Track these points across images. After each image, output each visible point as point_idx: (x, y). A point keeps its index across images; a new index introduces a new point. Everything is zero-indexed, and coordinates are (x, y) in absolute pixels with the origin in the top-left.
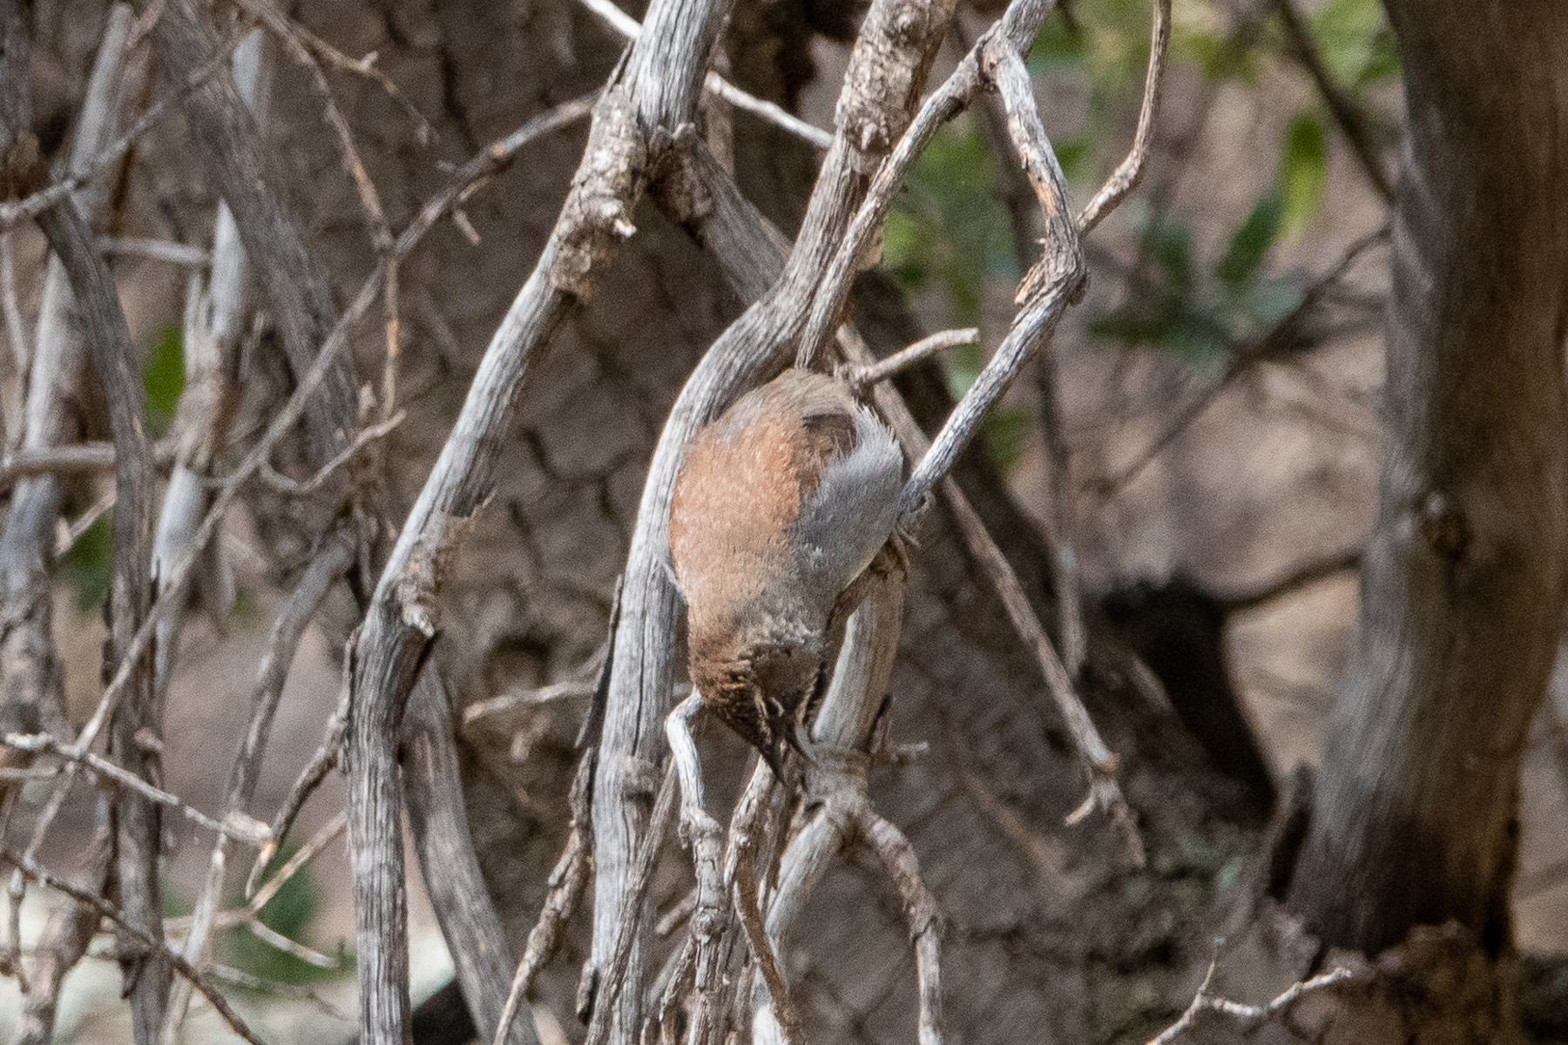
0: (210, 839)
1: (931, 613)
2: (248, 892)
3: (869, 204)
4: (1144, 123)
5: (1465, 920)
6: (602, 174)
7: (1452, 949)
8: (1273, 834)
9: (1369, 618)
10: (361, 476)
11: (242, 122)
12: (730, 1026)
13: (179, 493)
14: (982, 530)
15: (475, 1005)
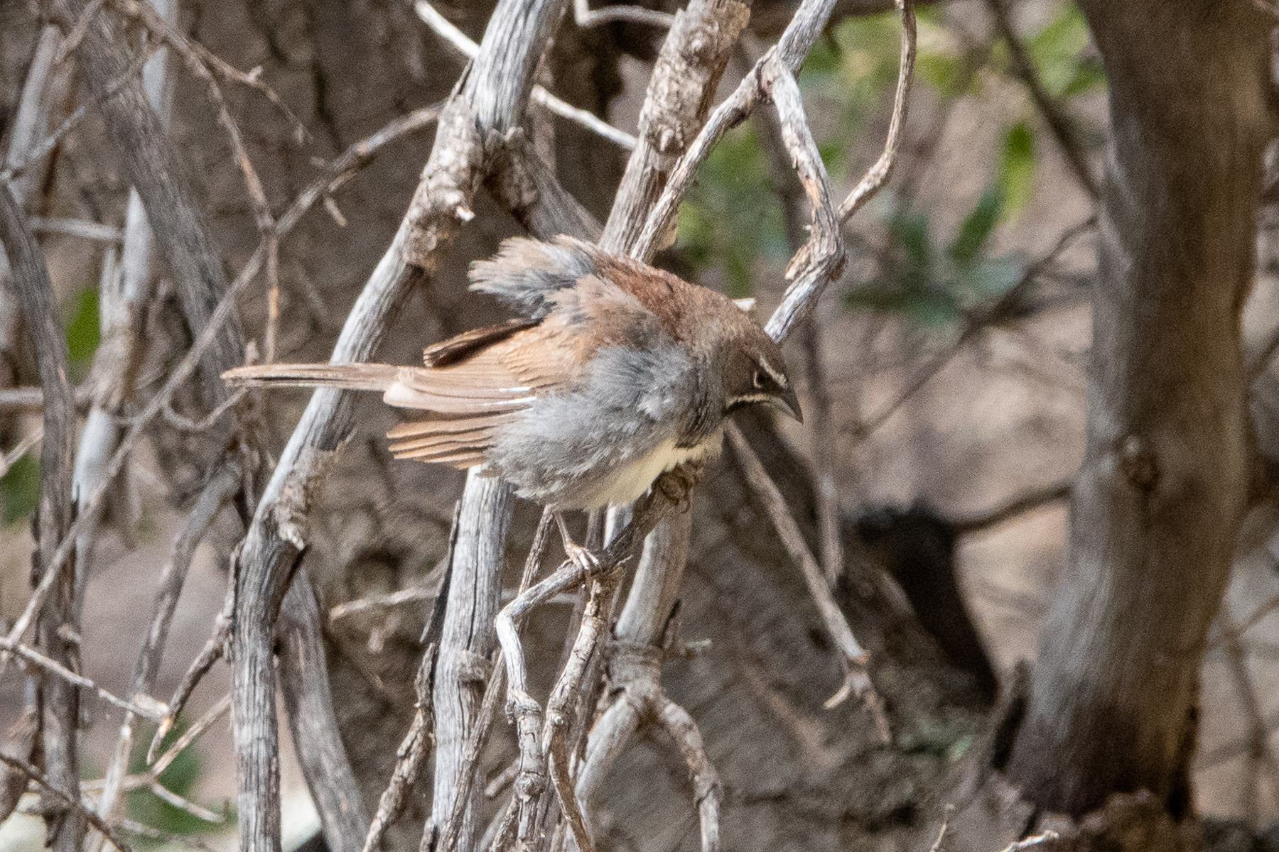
1: (714, 533)
2: (149, 760)
3: (667, 196)
4: (893, 130)
5: (1154, 790)
7: (1144, 813)
8: (996, 717)
9: (1078, 540)
10: (247, 417)
13: (93, 434)
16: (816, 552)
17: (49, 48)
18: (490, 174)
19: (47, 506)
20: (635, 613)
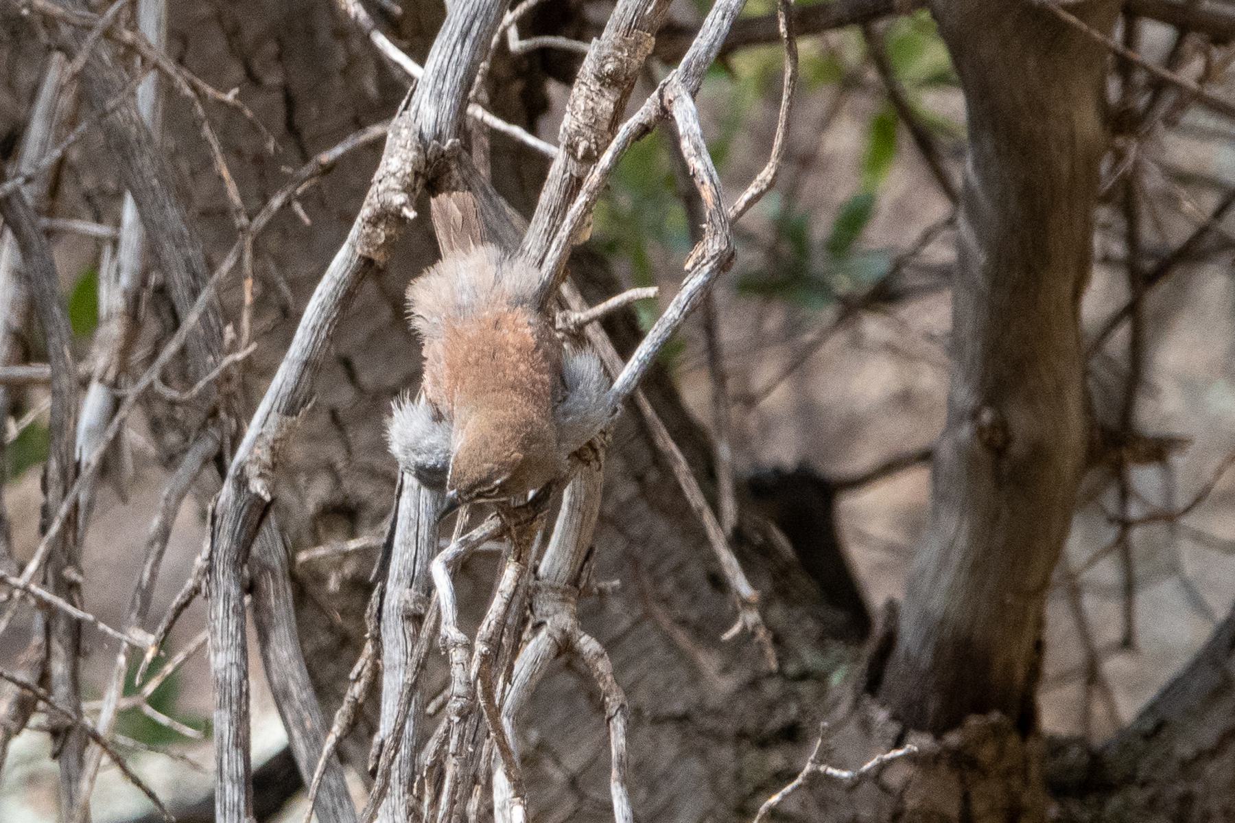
0: (115, 646)
1: (627, 490)
2: (138, 681)
3: (582, 198)
4: (777, 142)
5: (1005, 711)
6: (394, 174)
7: (996, 730)
8: (869, 649)
9: (939, 496)
10: (226, 388)
11: (143, 137)
12: (476, 781)
13: (94, 402)
14: (664, 431)
15: (303, 765)
16: (714, 505)
17: (57, 71)
18: (431, 177)
19: (54, 465)
20: (554, 558)
